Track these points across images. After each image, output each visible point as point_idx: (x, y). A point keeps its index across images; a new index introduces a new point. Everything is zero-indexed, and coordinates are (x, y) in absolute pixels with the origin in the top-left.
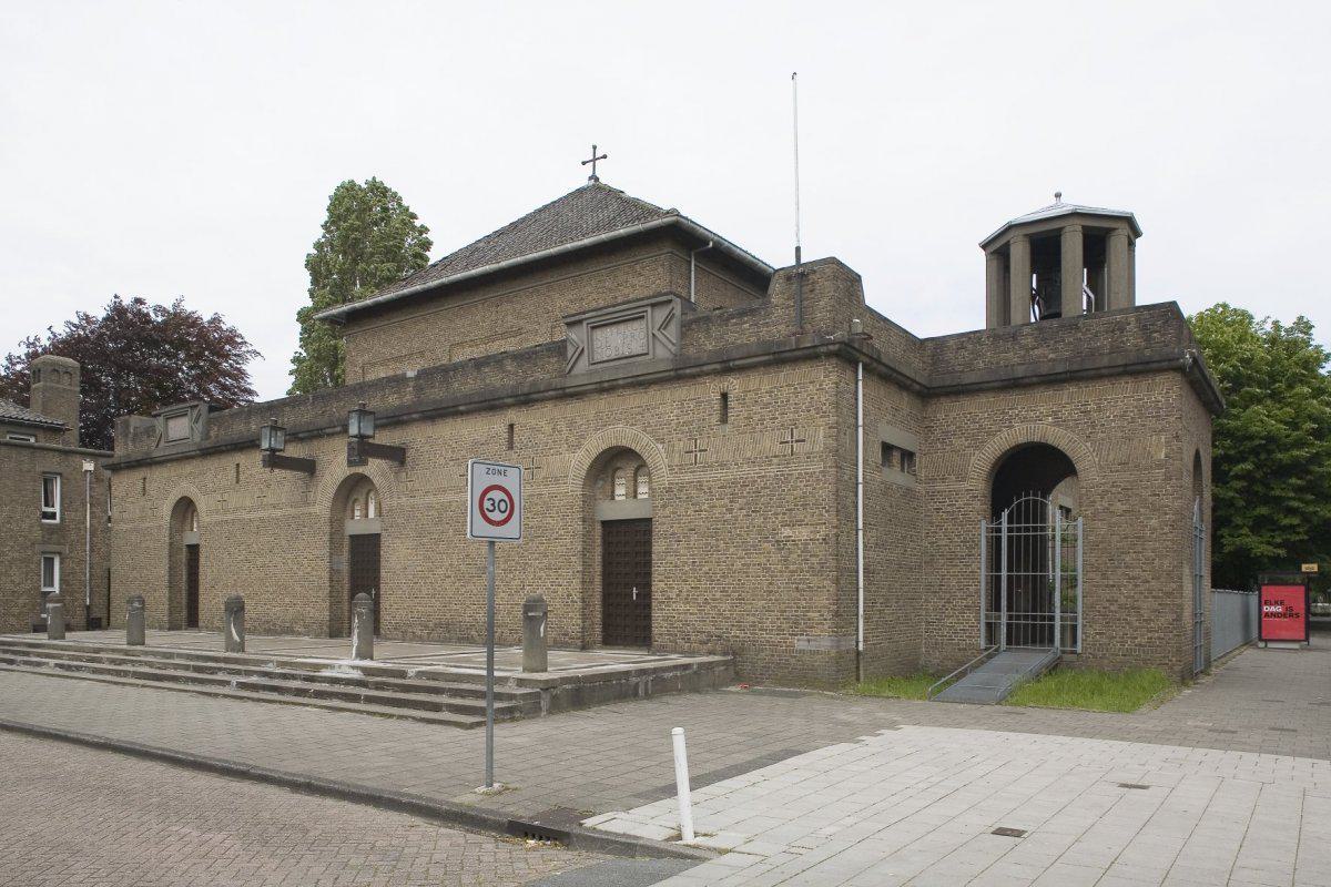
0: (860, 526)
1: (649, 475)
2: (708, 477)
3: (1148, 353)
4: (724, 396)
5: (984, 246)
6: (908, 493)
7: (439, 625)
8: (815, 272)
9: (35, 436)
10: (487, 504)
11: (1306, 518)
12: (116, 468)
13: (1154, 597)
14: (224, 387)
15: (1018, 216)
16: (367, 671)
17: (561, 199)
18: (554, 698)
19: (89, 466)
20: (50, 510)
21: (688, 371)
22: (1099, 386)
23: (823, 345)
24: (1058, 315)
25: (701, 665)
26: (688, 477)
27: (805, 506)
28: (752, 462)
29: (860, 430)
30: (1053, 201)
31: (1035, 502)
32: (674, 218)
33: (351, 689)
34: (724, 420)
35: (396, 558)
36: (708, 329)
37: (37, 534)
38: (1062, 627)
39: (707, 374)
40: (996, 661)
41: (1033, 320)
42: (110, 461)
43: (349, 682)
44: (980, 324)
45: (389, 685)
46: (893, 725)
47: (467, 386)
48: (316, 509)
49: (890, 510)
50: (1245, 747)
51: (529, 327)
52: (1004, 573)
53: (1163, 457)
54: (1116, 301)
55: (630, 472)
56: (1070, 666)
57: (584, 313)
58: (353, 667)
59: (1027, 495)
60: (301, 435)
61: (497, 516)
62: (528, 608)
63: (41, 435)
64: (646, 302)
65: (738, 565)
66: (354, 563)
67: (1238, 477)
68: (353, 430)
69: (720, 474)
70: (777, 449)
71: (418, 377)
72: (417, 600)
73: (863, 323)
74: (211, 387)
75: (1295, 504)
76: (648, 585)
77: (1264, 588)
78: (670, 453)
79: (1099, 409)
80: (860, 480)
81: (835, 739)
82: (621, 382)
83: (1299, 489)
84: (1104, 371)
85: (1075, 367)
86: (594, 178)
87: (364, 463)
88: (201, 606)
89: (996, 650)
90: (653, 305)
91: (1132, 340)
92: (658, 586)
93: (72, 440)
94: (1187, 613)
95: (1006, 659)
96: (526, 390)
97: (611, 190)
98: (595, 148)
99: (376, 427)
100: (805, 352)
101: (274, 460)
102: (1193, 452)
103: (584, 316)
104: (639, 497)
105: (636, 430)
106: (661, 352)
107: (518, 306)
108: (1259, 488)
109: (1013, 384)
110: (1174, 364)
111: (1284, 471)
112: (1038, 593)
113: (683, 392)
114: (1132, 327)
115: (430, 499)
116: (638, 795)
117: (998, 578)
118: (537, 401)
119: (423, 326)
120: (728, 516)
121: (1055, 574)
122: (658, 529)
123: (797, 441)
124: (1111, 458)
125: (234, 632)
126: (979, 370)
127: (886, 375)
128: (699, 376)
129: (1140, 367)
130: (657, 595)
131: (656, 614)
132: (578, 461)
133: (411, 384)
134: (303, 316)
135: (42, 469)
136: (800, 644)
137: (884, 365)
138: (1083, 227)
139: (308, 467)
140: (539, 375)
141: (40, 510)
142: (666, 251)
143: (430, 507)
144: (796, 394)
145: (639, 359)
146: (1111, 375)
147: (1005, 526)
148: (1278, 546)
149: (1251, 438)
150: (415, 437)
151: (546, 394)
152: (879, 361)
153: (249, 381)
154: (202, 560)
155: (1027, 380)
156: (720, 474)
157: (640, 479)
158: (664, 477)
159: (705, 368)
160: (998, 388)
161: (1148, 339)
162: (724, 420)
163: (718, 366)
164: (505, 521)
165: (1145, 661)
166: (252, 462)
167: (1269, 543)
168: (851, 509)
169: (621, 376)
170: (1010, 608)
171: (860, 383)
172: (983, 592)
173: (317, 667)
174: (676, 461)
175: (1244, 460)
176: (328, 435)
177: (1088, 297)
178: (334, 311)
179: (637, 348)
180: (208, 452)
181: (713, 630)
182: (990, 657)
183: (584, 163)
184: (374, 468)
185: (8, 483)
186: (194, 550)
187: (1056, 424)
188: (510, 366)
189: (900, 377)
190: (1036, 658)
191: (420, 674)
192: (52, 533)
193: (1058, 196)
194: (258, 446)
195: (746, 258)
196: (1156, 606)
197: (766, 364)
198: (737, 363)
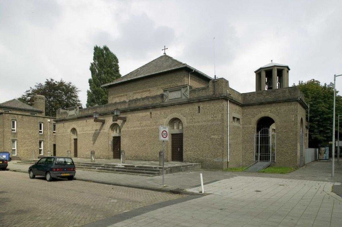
0: (228, 135)
1: (182, 124)
3: (290, 97)
4: (199, 107)
5: (255, 72)
7: (135, 156)
9: (36, 114)
10: (163, 134)
12: (57, 121)
14: (73, 100)
15: (264, 66)
18: (167, 171)
19: (49, 120)
21: (191, 102)
22: (280, 104)
23: (220, 97)
25: (195, 165)
26: (191, 124)
27: (217, 131)
28: (205, 121)
29: (228, 114)
30: (271, 62)
32: (186, 66)
33: (123, 169)
35: (124, 142)
36: (195, 93)
37: (38, 136)
38: (272, 156)
40: (257, 164)
41: (266, 89)
42: (56, 120)
43: (122, 168)
44: (253, 89)
46: (236, 176)
47: (140, 104)
48: (105, 131)
52: (259, 145)
53: (293, 119)
55: (178, 123)
58: (123, 165)
59: (264, 128)
61: (165, 136)
62: (160, 153)
64: (181, 87)
65: (202, 143)
67: (316, 121)
68: (115, 114)
69: (198, 124)
70: (211, 118)
71: (129, 101)
73: (229, 91)
74: (70, 100)
75: (329, 127)
76: (182, 148)
78: (187, 119)
79: (280, 109)
80: (228, 125)
82: (176, 104)
84: (281, 101)
85: (275, 100)
86: (165, 53)
87: (117, 121)
88: (78, 152)
89: (258, 161)
91: (287, 95)
92: (184, 148)
93: (44, 114)
94: (299, 154)
96: (154, 105)
97: (169, 57)
98: (165, 46)
99: (121, 113)
101: (96, 120)
105: (180, 114)
107: (149, 85)
108: (321, 123)
109: (261, 104)
112: (267, 149)
114: (287, 92)
115: (132, 129)
116: (191, 187)
117: (258, 146)
118: (157, 107)
119: (126, 89)
120: (200, 133)
121: (271, 145)
122: (184, 136)
124: (282, 120)
125: (93, 158)
126: (254, 100)
127: (233, 102)
129: (288, 100)
130: (184, 150)
133: (127, 103)
134: (90, 81)
136: (215, 160)
137: (233, 100)
138: (277, 69)
139: (103, 122)
141: (11, 129)
142: (183, 72)
143: (132, 131)
144: (215, 107)
145: (180, 99)
146: (282, 102)
147: (259, 134)
149: (319, 111)
152: (232, 100)
154: (78, 142)
155: (264, 103)
156: (198, 124)
157: (180, 125)
159: (195, 101)
160: (258, 104)
162: (199, 113)
163: (198, 101)
164: (166, 137)
166: (92, 121)
168: (227, 132)
169: (176, 102)
170: (260, 153)
171: (228, 105)
172: (255, 149)
176: (108, 114)
178: (106, 85)
179: (179, 96)
182: (256, 163)
184: (119, 122)
187: (271, 113)
188: (150, 100)
189: (237, 103)
190: (265, 164)
191: (138, 167)
192: (41, 136)
193: (272, 61)
194: (93, 116)
195: (201, 73)
197: (208, 100)
198: (202, 100)
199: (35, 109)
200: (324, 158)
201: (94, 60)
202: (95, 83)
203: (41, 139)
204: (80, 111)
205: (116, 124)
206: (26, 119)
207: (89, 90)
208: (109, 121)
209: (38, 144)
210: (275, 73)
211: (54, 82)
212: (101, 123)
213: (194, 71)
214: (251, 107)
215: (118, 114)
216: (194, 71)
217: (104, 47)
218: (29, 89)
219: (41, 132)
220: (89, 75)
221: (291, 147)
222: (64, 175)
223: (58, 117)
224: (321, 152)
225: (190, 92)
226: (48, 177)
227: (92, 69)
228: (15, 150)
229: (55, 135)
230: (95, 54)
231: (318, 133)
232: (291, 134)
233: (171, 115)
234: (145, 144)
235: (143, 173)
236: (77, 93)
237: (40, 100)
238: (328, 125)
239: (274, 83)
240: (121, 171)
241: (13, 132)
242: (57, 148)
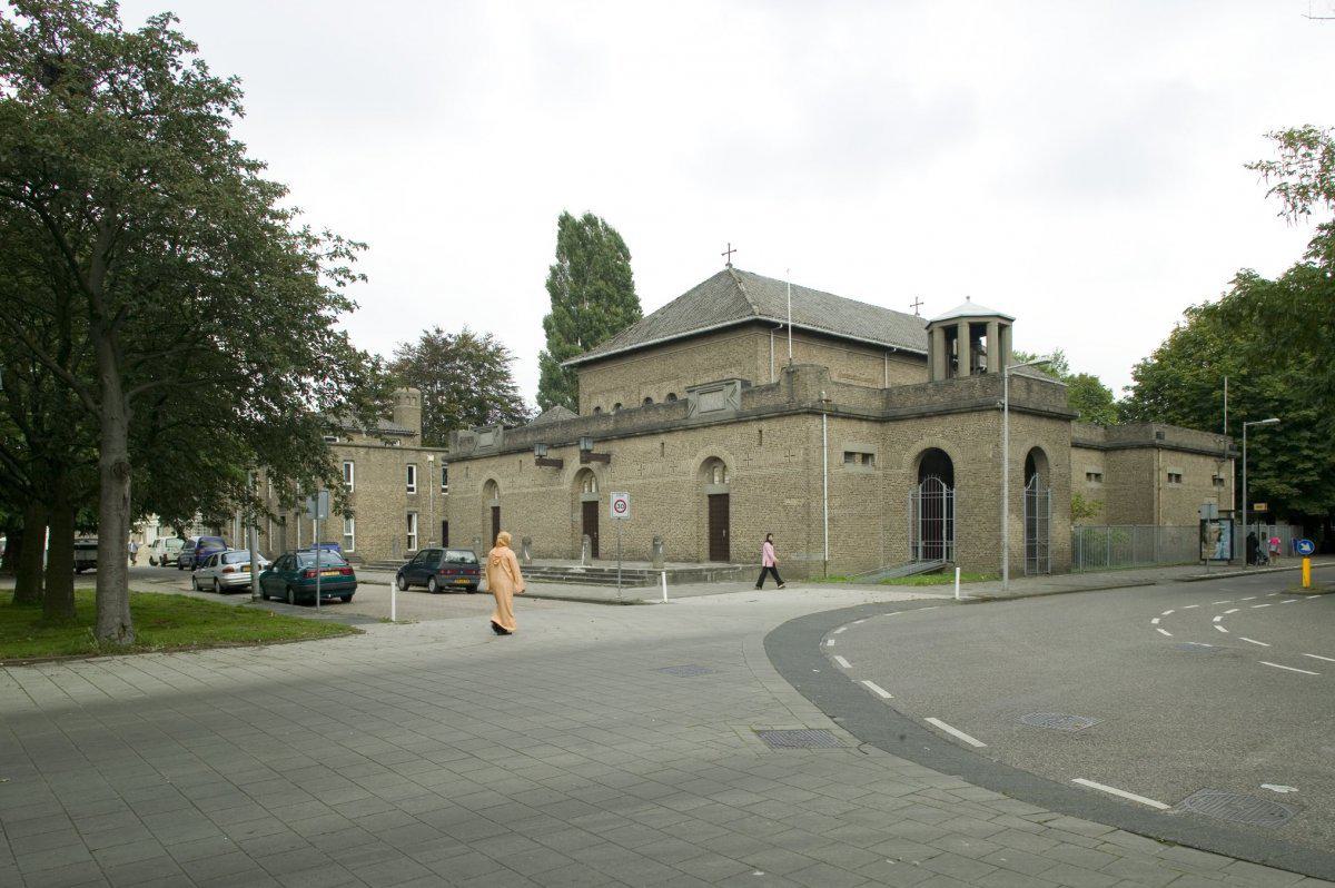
6: (868, 477)
11: (1318, 462)
12: (450, 461)
14: (498, 387)
16: (588, 570)
19: (431, 458)
20: (411, 486)
22: (962, 417)
35: (608, 514)
51: (682, 374)
52: (945, 519)
63: (402, 439)
66: (585, 517)
75: (1306, 452)
83: (1311, 440)
90: (727, 384)
101: (541, 462)
106: (730, 409)
108: (1282, 439)
113: (742, 429)
117: (948, 517)
122: (732, 500)
131: (732, 544)
132: (694, 463)
134: (547, 325)
136: (793, 557)
139: (559, 464)
150: (616, 448)
153: (513, 380)
158: (733, 472)
166: (529, 459)
173: (566, 569)
180: (503, 453)
184: (593, 465)
186: (496, 510)
188: (662, 411)
193: (968, 298)
197: (779, 416)
199: (395, 427)
200: (1218, 556)
201: (558, 257)
202: (561, 331)
203: (411, 509)
204: (505, 436)
205: (588, 470)
207: (545, 350)
208: (574, 463)
209: (405, 521)
210: (964, 333)
211: (444, 335)
214: (901, 424)
215: (589, 446)
217: (585, 218)
219: (412, 489)
220: (544, 306)
221: (988, 524)
222: (460, 582)
223: (453, 450)
224: (1207, 535)
225: (743, 395)
226: (432, 585)
227: (553, 288)
228: (351, 537)
229: (446, 498)
230: (560, 237)
231: (1271, 473)
232: (987, 491)
233: (705, 449)
234: (650, 521)
235: (608, 582)
236: (507, 363)
237: (407, 400)
238: (1305, 444)
239: (1007, 343)
240: (576, 580)
242: (451, 532)
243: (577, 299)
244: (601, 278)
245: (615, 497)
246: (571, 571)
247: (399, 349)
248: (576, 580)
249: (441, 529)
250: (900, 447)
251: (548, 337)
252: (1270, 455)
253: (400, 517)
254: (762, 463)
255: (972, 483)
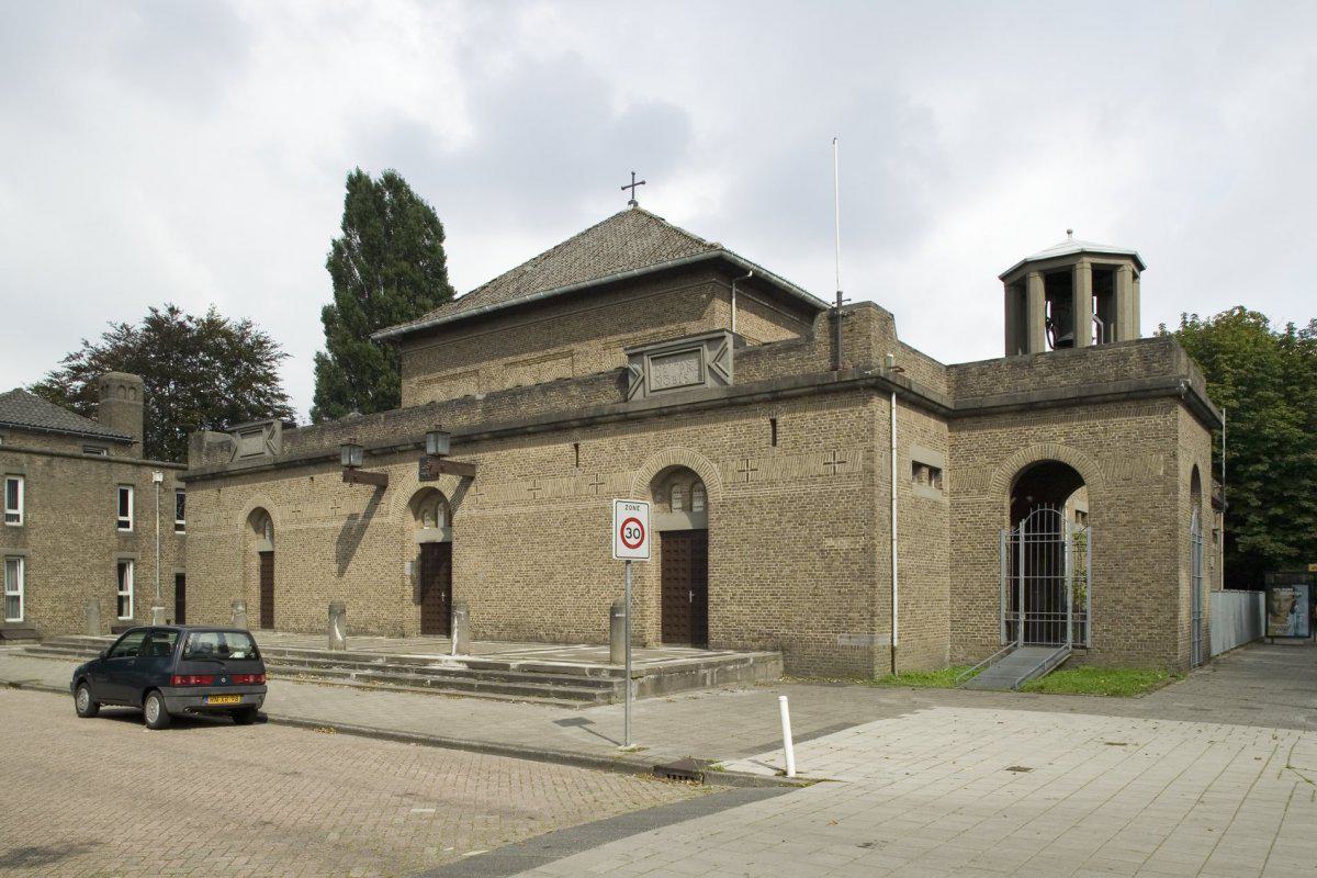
2: (758, 493)
5: (1003, 278)
8: (854, 314)
10: (626, 533)
12: (192, 481)
13: (1154, 598)
14: (260, 394)
16: (469, 664)
17: (602, 223)
19: (158, 477)
24: (1069, 344)
26: (741, 493)
27: (846, 519)
28: (796, 480)
31: (1050, 513)
33: (460, 679)
34: (774, 444)
36: (757, 363)
37: (114, 541)
39: (758, 402)
42: (186, 474)
45: (495, 676)
49: (918, 520)
50: (1214, 720)
52: (1022, 576)
53: (1161, 473)
54: (1127, 335)
55: (686, 488)
56: (1081, 659)
57: (645, 346)
58: (459, 662)
60: (374, 452)
61: (633, 541)
69: (768, 491)
70: (821, 469)
71: (487, 400)
72: (487, 604)
74: (246, 395)
77: (263, 709)
78: (724, 471)
79: (1106, 430)
81: (881, 716)
82: (679, 408)
87: (435, 477)
89: (1015, 646)
91: (1135, 370)
95: (1023, 652)
98: (633, 174)
99: (453, 445)
100: (846, 384)
102: (1191, 467)
103: (644, 349)
104: (695, 510)
108: (1275, 489)
110: (1173, 392)
111: (1292, 472)
114: (1134, 357)
123: (839, 463)
124: (1116, 475)
126: (1000, 392)
128: (750, 404)
130: (712, 599)
131: (712, 615)
135: (118, 481)
139: (382, 485)
140: (604, 400)
141: (3, 511)
143: (499, 519)
144: (838, 421)
146: (1117, 401)
147: (1022, 534)
148: (1291, 544)
149: (1266, 439)
151: (609, 418)
152: (910, 391)
154: (277, 567)
156: (768, 491)
157: (696, 494)
159: (756, 397)
161: (1148, 369)
163: (768, 396)
165: (1146, 655)
166: (336, 477)
167: (1283, 542)
170: (1027, 609)
173: (426, 662)
174: (730, 479)
175: (1259, 461)
177: (1098, 325)
179: (693, 378)
181: (764, 629)
182: (1009, 652)
183: (623, 189)
185: (89, 493)
190: (1046, 655)
191: (521, 667)
192: (125, 541)
193: (1069, 232)
194: (339, 460)
196: (1155, 606)
199: (101, 430)
200: (1291, 632)
201: (344, 229)
205: (435, 492)
206: (63, 470)
207: (324, 350)
209: (113, 573)
210: (1084, 280)
211: (181, 318)
212: (374, 488)
213: (751, 273)
216: (751, 273)
218: (79, 348)
219: (126, 524)
223: (195, 464)
224: (1276, 605)
225: (738, 358)
227: (337, 267)
228: (18, 598)
231: (1263, 529)
237: (121, 392)
241: (8, 523)
242: (189, 589)
243: (370, 283)
244: (405, 258)
245: (621, 512)
246: (436, 667)
247: (112, 331)
248: (451, 685)
249: (174, 586)
250: (980, 460)
251: (328, 333)
252: (1261, 507)
253: (104, 567)
254: (776, 475)
255: (1124, 518)
